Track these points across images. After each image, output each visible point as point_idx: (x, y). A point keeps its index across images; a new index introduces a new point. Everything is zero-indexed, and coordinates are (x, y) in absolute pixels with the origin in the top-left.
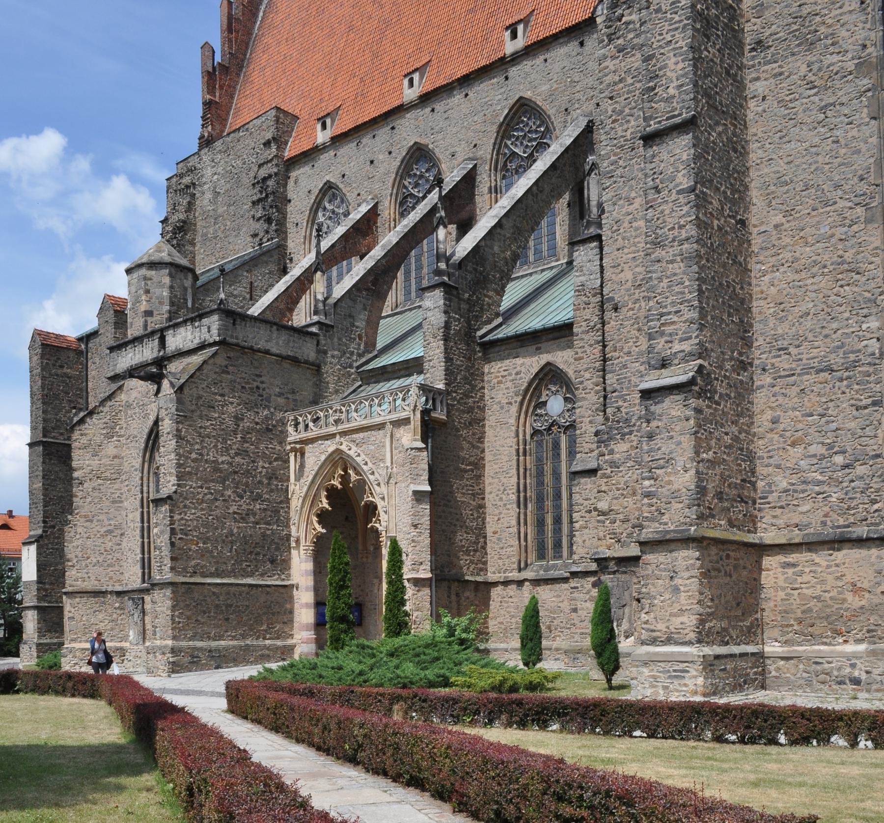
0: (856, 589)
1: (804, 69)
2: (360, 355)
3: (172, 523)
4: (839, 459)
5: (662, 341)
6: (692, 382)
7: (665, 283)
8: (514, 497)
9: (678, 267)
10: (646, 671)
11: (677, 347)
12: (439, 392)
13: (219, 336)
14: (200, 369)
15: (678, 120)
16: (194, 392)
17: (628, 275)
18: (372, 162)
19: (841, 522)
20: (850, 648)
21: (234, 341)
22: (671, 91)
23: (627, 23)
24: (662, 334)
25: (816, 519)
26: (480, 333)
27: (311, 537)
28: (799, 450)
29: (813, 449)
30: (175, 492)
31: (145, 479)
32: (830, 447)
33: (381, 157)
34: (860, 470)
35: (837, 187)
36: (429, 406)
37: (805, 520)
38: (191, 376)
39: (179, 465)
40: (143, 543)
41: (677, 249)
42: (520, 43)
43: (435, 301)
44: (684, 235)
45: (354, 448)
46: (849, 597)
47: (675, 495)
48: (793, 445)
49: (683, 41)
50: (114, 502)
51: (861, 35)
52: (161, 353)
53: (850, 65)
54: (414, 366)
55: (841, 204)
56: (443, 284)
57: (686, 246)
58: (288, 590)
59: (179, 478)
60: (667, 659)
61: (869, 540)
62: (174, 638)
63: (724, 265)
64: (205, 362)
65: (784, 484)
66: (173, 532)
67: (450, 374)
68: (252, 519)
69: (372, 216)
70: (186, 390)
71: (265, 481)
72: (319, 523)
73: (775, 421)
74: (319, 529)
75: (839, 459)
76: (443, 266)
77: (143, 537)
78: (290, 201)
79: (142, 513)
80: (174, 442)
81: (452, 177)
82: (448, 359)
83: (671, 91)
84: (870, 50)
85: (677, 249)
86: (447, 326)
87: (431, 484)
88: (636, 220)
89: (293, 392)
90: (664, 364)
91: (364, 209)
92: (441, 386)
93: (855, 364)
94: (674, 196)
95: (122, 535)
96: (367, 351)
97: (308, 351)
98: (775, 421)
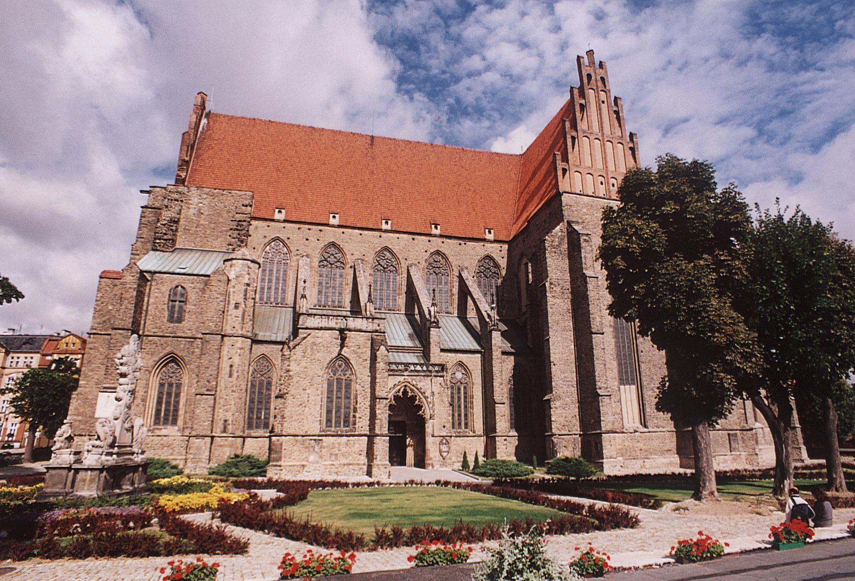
33: (313, 240)
42: (389, 227)
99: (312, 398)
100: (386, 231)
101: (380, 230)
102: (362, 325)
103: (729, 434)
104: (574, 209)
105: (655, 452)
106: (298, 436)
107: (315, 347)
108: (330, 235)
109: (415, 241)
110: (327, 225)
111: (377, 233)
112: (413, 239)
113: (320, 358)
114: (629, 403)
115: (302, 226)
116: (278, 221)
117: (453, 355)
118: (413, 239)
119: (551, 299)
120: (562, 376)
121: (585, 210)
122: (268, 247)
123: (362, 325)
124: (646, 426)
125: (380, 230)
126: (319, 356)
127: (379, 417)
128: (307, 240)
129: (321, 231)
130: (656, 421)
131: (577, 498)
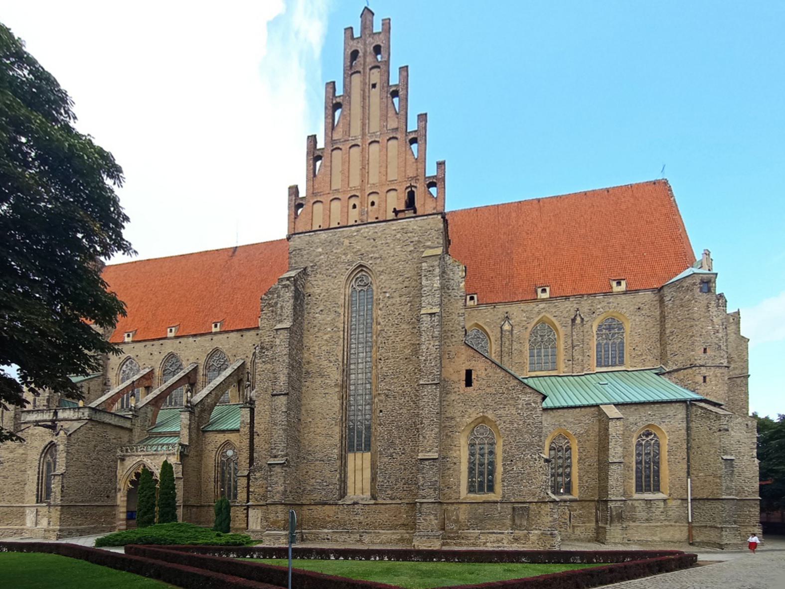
0: (329, 517)
1: (320, 382)
2: (149, 427)
3: (63, 483)
4: (325, 484)
5: (275, 451)
6: (284, 463)
7: (277, 435)
8: (213, 480)
9: (281, 432)
10: (268, 538)
11: (279, 453)
12: (186, 446)
13: (88, 417)
14: (79, 428)
15: (283, 393)
16: (76, 437)
17: (262, 426)
18: (151, 354)
19: (325, 499)
20: (326, 531)
21: (95, 419)
22: (281, 384)
23: (266, 355)
24: (275, 449)
25: (318, 498)
26: (202, 427)
27: (126, 489)
28: (314, 480)
29: (317, 481)
30: (65, 472)
31: (41, 464)
32: (323, 480)
33: (156, 353)
34: (331, 487)
35: (327, 414)
36: (182, 450)
37: (315, 498)
38: (76, 431)
39: (67, 463)
40: (38, 488)
41: (280, 427)
42: (218, 329)
43: (185, 417)
44: (283, 423)
45: (149, 461)
46: (327, 518)
47: (278, 492)
48: (312, 479)
49: (286, 372)
50: (21, 471)
51: (337, 377)
52: (54, 418)
53: (333, 384)
54: (176, 434)
55: (328, 419)
56: (189, 411)
57: (283, 427)
58: (114, 506)
59: (67, 467)
60: (275, 535)
61: (332, 504)
62: (60, 526)
63: (294, 431)
64: (81, 426)
65: (309, 489)
66: (63, 487)
67: (190, 439)
68: (100, 482)
69: (149, 376)
70: (72, 436)
71: (106, 468)
72: (131, 484)
73: (307, 472)
74: (130, 486)
75: (325, 484)
76: (189, 405)
77: (38, 485)
78: (109, 359)
79: (39, 477)
80: (65, 454)
81: (187, 368)
82: (190, 435)
83: (281, 384)
84: (339, 381)
85: (280, 427)
86: (190, 425)
87: (183, 475)
88: (266, 411)
89: (120, 438)
90: (275, 457)
91: (147, 370)
92: (187, 444)
93: (330, 460)
94: (280, 413)
95: (25, 484)
96: (152, 425)
97: (128, 424)
98: (307, 472)
99: (31, 477)
100: (216, 333)
101: (211, 333)
102: (69, 415)
103: (514, 509)
104: (305, 252)
105: (382, 526)
106: (711, 527)
107: (33, 438)
108: (169, 347)
109: (244, 337)
110: (166, 338)
111: (209, 337)
112: (242, 336)
113: (36, 446)
114: (359, 473)
115: (147, 343)
116: (128, 343)
117: (221, 435)
118: (242, 336)
119: (260, 366)
120: (267, 446)
121: (320, 250)
122: (125, 366)
123: (69, 415)
124: (375, 499)
125: (211, 333)
126: (36, 444)
127: (53, 490)
128: (151, 354)
129: (162, 344)
130: (390, 492)
131: (513, 577)
